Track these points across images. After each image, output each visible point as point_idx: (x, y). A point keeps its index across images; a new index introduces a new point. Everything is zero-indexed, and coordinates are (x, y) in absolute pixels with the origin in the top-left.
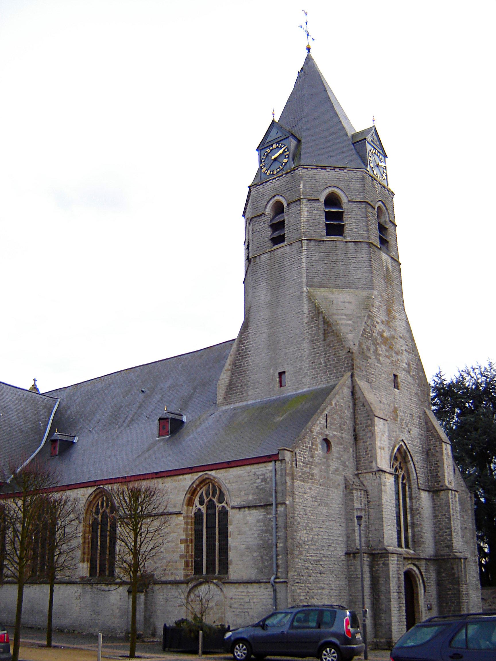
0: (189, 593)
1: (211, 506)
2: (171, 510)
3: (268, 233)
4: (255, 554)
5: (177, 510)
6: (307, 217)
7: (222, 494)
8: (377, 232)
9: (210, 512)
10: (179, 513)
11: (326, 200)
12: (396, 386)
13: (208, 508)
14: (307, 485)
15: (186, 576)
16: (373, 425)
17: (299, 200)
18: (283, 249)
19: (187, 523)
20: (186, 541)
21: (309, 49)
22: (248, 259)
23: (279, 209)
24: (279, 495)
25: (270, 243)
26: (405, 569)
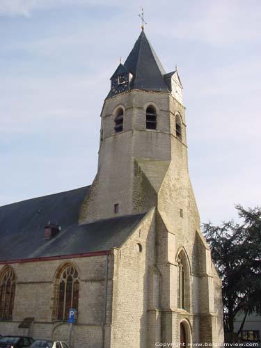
0: (54, 329)
1: (70, 279)
2: (47, 280)
3: (113, 125)
4: (94, 309)
5: (50, 280)
6: (137, 117)
7: (76, 273)
8: (175, 128)
9: (69, 282)
10: (51, 282)
11: (147, 109)
12: (181, 216)
13: (68, 280)
14: (126, 270)
15: (53, 319)
16: (166, 237)
17: (132, 108)
18: (120, 135)
19: (55, 288)
20: (54, 298)
21: (143, 28)
22: (102, 140)
23: (121, 112)
24: (109, 275)
25: (114, 131)
26: (181, 321)
